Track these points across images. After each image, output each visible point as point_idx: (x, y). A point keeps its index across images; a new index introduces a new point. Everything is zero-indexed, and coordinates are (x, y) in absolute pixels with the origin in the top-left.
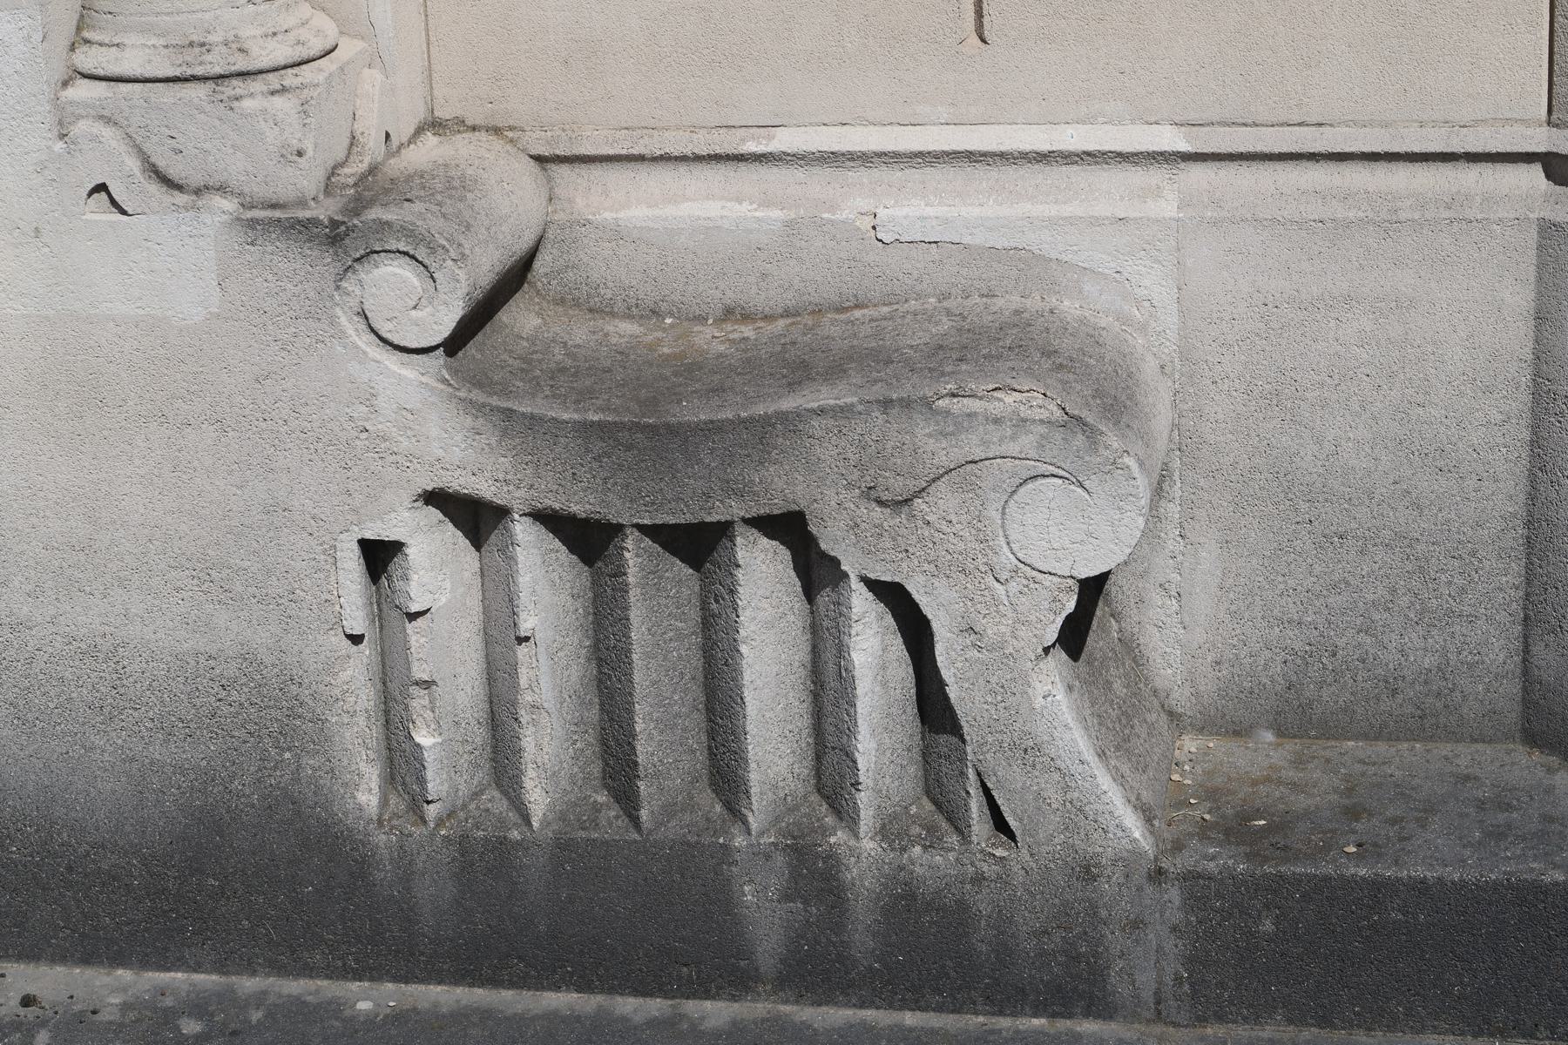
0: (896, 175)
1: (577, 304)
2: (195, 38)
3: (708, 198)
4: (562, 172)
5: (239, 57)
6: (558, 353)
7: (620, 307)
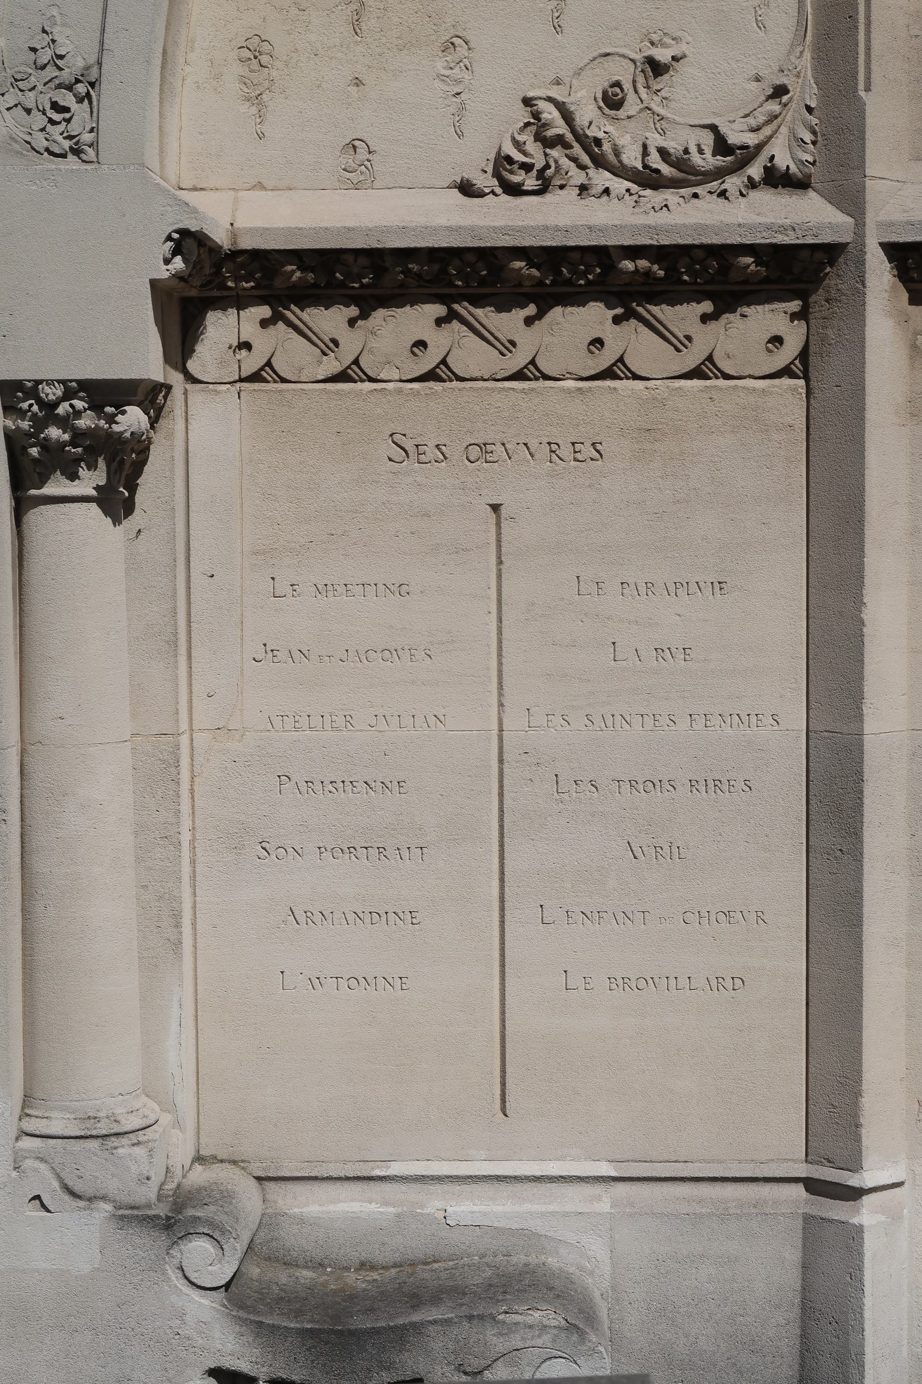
0: (457, 1188)
1: (277, 1260)
2: (91, 1114)
5: (115, 1125)
6: (276, 1289)
7: (301, 1262)
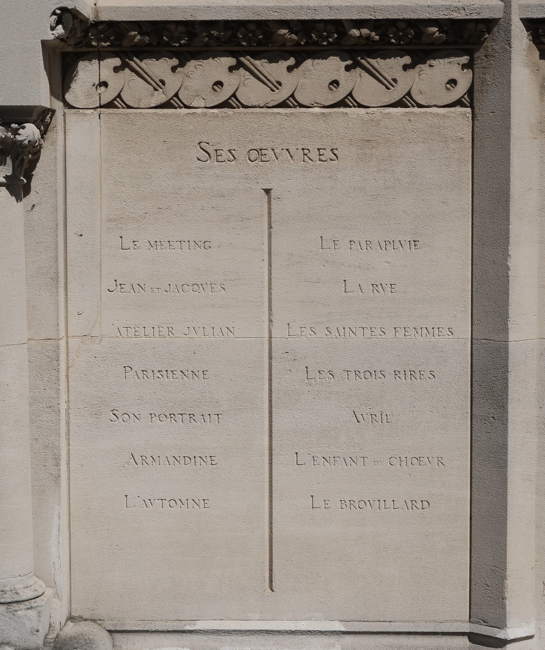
0: (240, 638)
3: (171, 646)
4: (118, 636)
5: (16, 596)
